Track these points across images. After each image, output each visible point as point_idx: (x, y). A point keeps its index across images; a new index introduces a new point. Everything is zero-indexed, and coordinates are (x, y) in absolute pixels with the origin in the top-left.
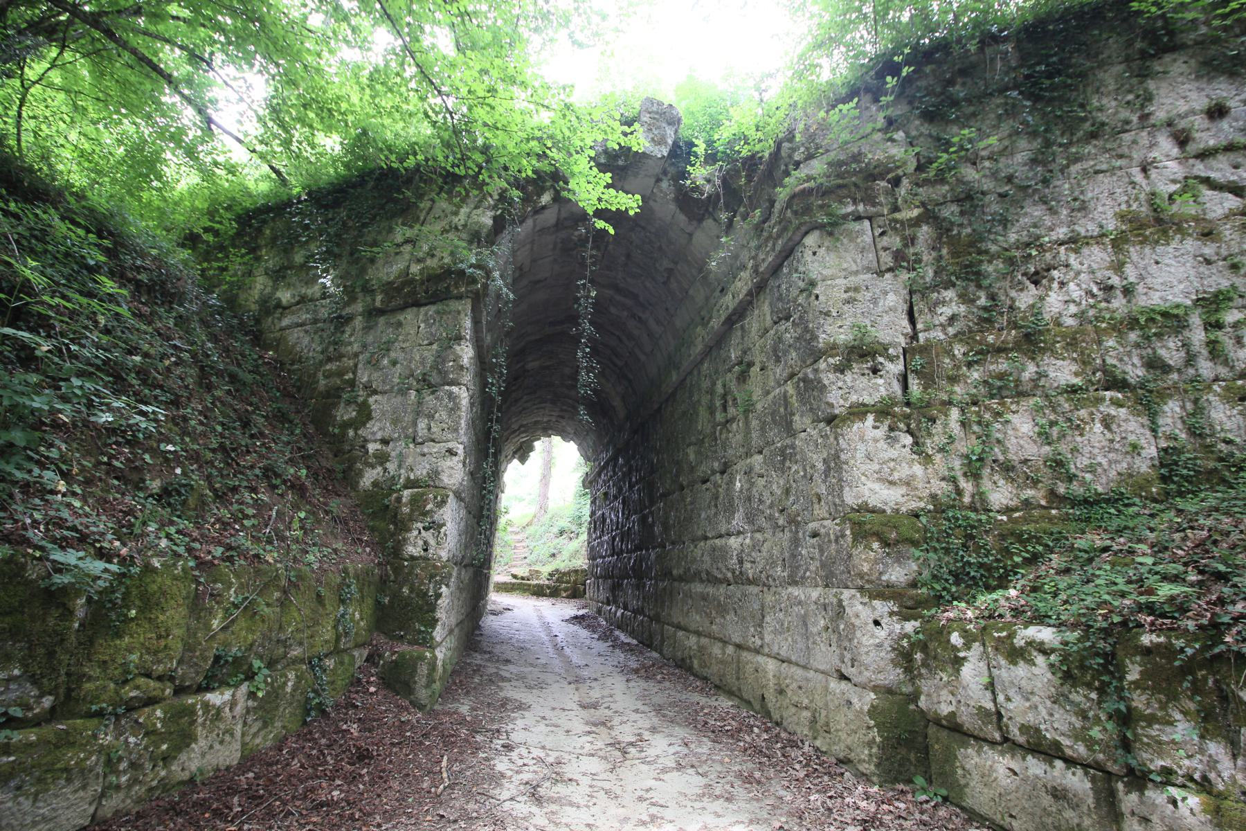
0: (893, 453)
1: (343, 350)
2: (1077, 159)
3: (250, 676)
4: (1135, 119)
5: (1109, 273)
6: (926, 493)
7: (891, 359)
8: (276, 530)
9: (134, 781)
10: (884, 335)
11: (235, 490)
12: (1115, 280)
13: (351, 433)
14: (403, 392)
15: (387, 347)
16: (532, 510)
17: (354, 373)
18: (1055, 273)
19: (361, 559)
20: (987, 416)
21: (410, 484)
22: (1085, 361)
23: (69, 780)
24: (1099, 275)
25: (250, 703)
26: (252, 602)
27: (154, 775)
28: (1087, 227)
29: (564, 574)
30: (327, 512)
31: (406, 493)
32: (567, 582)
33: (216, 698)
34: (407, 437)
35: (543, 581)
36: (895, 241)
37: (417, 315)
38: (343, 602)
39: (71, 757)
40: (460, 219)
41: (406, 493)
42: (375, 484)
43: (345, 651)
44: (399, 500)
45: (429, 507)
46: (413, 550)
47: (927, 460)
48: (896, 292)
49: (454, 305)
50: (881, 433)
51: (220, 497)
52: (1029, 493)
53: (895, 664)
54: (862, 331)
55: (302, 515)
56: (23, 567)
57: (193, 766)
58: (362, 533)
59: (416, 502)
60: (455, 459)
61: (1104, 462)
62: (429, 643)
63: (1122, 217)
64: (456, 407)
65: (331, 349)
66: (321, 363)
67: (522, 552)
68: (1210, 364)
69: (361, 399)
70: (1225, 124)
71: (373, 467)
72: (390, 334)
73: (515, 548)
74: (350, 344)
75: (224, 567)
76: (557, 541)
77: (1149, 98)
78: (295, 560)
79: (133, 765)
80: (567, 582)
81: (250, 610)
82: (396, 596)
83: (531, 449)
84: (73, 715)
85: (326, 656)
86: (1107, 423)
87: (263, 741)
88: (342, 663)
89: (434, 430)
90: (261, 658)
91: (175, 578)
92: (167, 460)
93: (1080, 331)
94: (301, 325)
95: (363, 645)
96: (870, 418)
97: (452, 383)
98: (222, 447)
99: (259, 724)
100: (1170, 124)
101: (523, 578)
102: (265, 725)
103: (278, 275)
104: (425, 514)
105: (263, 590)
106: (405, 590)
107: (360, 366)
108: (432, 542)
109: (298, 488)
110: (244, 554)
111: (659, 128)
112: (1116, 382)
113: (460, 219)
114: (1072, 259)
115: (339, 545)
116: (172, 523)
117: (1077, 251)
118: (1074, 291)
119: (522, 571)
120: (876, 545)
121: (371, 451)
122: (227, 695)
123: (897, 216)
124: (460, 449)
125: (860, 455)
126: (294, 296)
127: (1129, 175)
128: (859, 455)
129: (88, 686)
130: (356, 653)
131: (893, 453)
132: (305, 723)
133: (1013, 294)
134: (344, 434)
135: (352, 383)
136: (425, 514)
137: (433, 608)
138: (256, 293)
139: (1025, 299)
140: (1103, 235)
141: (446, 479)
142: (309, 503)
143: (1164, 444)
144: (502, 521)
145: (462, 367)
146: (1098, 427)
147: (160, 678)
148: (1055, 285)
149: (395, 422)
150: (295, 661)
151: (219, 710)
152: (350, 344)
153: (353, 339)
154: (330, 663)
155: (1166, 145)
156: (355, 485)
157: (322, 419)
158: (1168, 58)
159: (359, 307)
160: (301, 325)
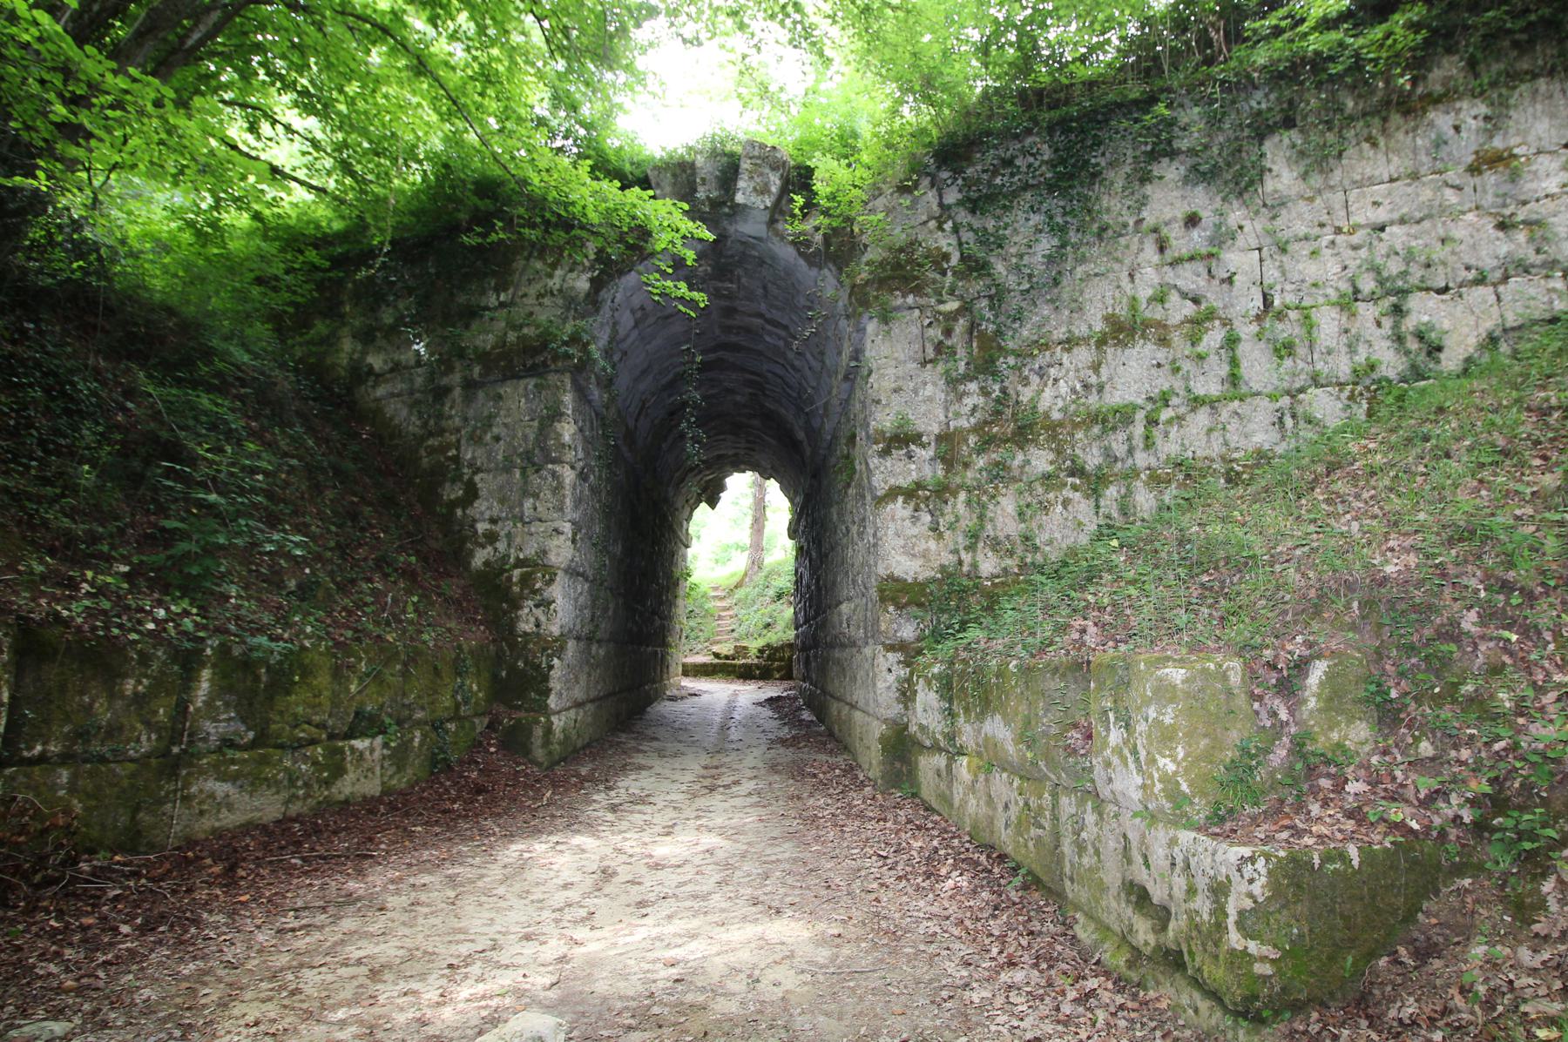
0: (915, 531)
1: (444, 423)
3: (383, 732)
4: (1131, 223)
5: (1090, 372)
6: (936, 565)
8: (393, 615)
9: (307, 796)
10: (921, 426)
12: (1093, 380)
13: (459, 512)
15: (488, 422)
16: (740, 563)
17: (458, 449)
19: (474, 638)
20: (984, 498)
21: (520, 563)
23: (269, 787)
24: (1082, 374)
25: (385, 752)
26: (380, 672)
28: (1081, 330)
30: (439, 595)
31: (517, 573)
32: (781, 659)
33: (360, 744)
34: (514, 517)
36: (936, 333)
37: (516, 388)
38: (459, 674)
39: (269, 772)
40: (555, 283)
41: (517, 573)
42: (487, 563)
43: (465, 718)
44: (510, 579)
45: (538, 586)
46: (526, 626)
47: (940, 536)
49: (553, 378)
50: (908, 512)
51: (342, 588)
52: (1009, 562)
54: (904, 420)
55: (415, 599)
56: (230, 648)
57: (347, 791)
58: (476, 613)
59: (526, 580)
60: (562, 538)
62: (544, 709)
64: (560, 486)
65: (432, 422)
66: (422, 439)
67: (728, 623)
68: (1145, 455)
69: (466, 477)
70: (1195, 233)
71: (484, 547)
72: (490, 407)
73: (720, 618)
74: (450, 417)
75: (355, 646)
76: (773, 606)
78: (412, 639)
79: (306, 785)
80: (781, 659)
81: (378, 678)
82: (513, 669)
83: (722, 488)
84: (266, 746)
85: (448, 721)
87: (400, 782)
88: (463, 727)
89: (540, 509)
90: (390, 716)
91: (321, 654)
92: (297, 563)
93: (1061, 424)
94: (399, 395)
95: (483, 714)
96: (900, 499)
98: (339, 545)
99: (394, 768)
100: (1155, 230)
101: (727, 657)
103: (367, 337)
104: (535, 592)
105: (387, 663)
106: (521, 664)
107: (463, 442)
108: (543, 618)
109: (409, 574)
110: (369, 635)
111: (761, 174)
113: (555, 283)
114: (1065, 358)
115: (452, 624)
116: (310, 614)
117: (1069, 350)
118: (1063, 388)
119: (726, 649)
120: (891, 609)
121: (480, 531)
122: (367, 743)
124: (567, 528)
126: (385, 362)
127: (1118, 279)
128: (890, 532)
129: (273, 727)
130: (476, 721)
131: (915, 531)
132: (432, 773)
133: (1020, 388)
134: (452, 513)
136: (535, 592)
137: (546, 678)
138: (344, 360)
140: (1090, 337)
141: (553, 559)
142: (421, 587)
145: (563, 445)
147: (317, 726)
148: (1050, 383)
149: (502, 501)
150: (419, 723)
151: (362, 754)
152: (450, 417)
153: (454, 409)
154: (452, 726)
155: (1150, 252)
159: (456, 378)
160: (399, 395)
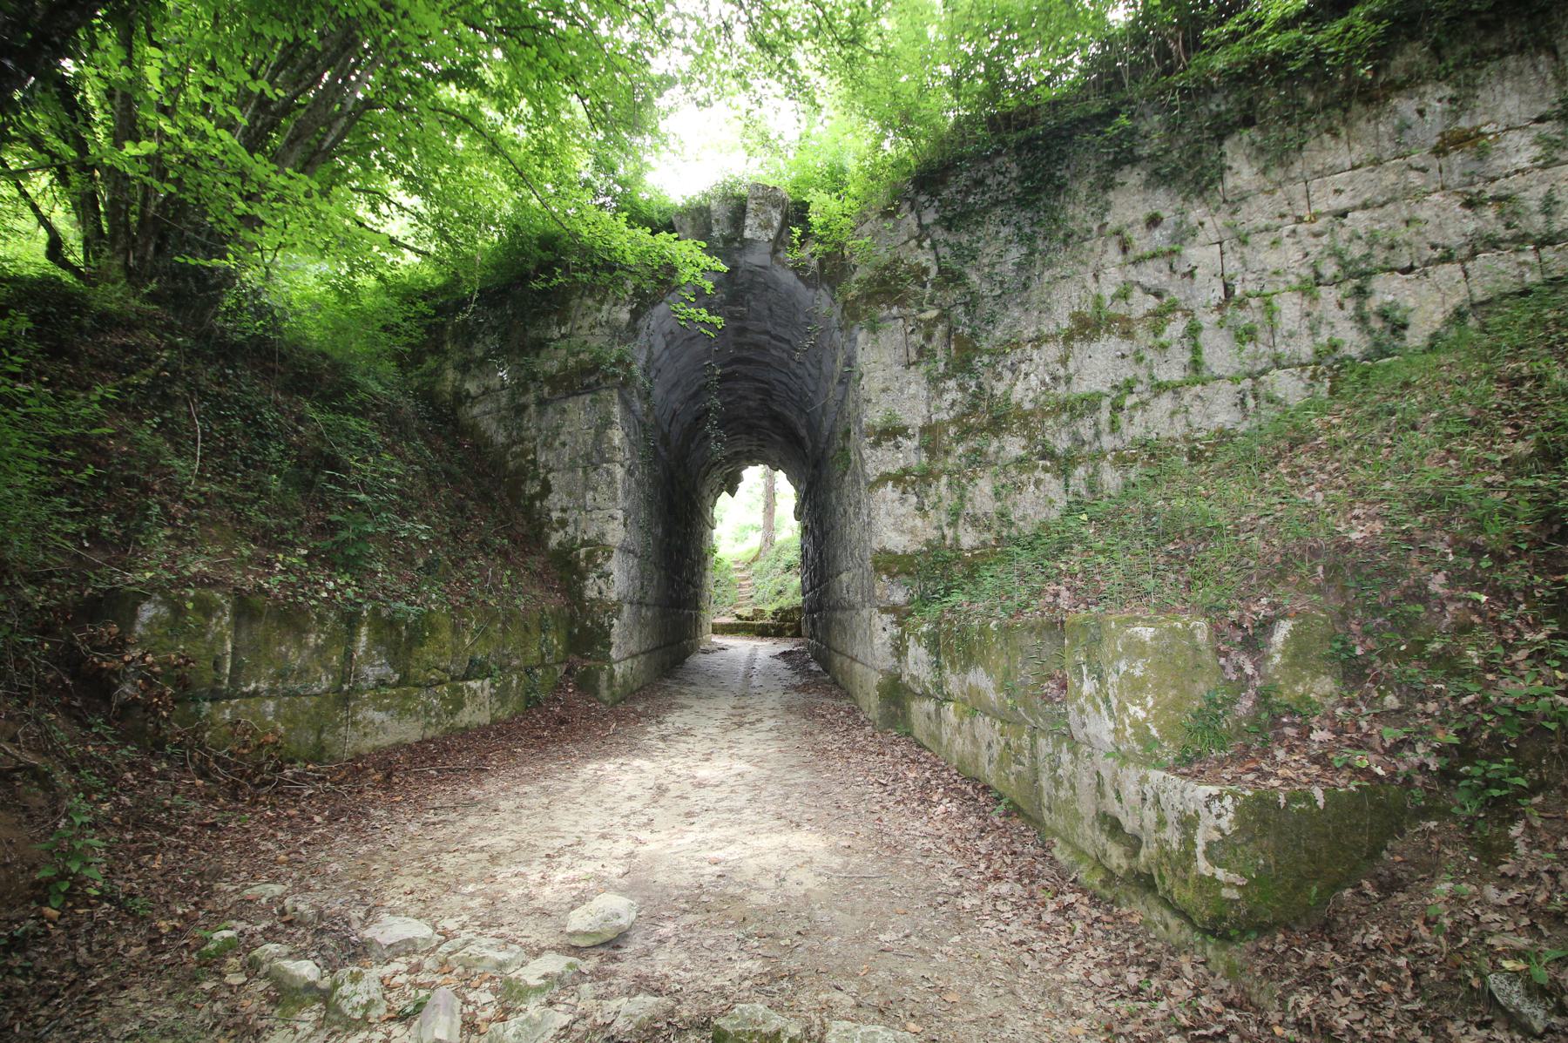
0: (903, 510)
2: (1051, 265)
7: (909, 437)
11: (463, 559)
12: (1062, 372)
13: (538, 504)
14: (572, 469)
16: (755, 541)
18: (1023, 366)
21: (585, 543)
22: (1030, 438)
27: (448, 722)
28: (1049, 328)
29: (787, 612)
31: (583, 551)
35: (768, 621)
39: (411, 704)
40: (603, 316)
41: (583, 551)
42: (560, 544)
46: (591, 593)
47: (926, 514)
48: (918, 383)
49: (604, 393)
50: (897, 495)
51: (455, 565)
53: (892, 655)
54: (891, 416)
57: (466, 720)
59: (590, 557)
61: (1031, 513)
63: (1073, 316)
66: (508, 447)
67: (747, 591)
77: (1107, 207)
82: (583, 628)
86: (1038, 483)
96: (890, 484)
97: (608, 461)
98: (452, 531)
100: (1118, 233)
102: (503, 705)
103: (464, 368)
104: (597, 566)
106: (588, 623)
108: (604, 587)
109: (505, 554)
112: (1048, 454)
113: (603, 316)
118: (1034, 381)
119: (746, 612)
120: (884, 577)
122: (479, 683)
123: (923, 316)
124: (620, 514)
125: (882, 512)
127: (1084, 280)
131: (903, 510)
135: (534, 462)
136: (597, 566)
137: (608, 635)
139: (1000, 388)
143: (1071, 499)
144: (712, 560)
146: (1032, 488)
149: (569, 494)
150: (515, 669)
153: (530, 422)
154: (539, 672)
156: (545, 546)
157: (515, 491)
158: (1127, 168)
